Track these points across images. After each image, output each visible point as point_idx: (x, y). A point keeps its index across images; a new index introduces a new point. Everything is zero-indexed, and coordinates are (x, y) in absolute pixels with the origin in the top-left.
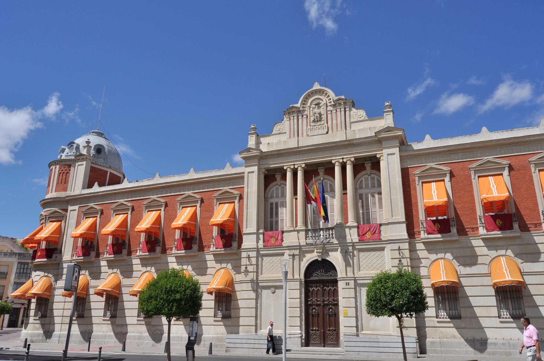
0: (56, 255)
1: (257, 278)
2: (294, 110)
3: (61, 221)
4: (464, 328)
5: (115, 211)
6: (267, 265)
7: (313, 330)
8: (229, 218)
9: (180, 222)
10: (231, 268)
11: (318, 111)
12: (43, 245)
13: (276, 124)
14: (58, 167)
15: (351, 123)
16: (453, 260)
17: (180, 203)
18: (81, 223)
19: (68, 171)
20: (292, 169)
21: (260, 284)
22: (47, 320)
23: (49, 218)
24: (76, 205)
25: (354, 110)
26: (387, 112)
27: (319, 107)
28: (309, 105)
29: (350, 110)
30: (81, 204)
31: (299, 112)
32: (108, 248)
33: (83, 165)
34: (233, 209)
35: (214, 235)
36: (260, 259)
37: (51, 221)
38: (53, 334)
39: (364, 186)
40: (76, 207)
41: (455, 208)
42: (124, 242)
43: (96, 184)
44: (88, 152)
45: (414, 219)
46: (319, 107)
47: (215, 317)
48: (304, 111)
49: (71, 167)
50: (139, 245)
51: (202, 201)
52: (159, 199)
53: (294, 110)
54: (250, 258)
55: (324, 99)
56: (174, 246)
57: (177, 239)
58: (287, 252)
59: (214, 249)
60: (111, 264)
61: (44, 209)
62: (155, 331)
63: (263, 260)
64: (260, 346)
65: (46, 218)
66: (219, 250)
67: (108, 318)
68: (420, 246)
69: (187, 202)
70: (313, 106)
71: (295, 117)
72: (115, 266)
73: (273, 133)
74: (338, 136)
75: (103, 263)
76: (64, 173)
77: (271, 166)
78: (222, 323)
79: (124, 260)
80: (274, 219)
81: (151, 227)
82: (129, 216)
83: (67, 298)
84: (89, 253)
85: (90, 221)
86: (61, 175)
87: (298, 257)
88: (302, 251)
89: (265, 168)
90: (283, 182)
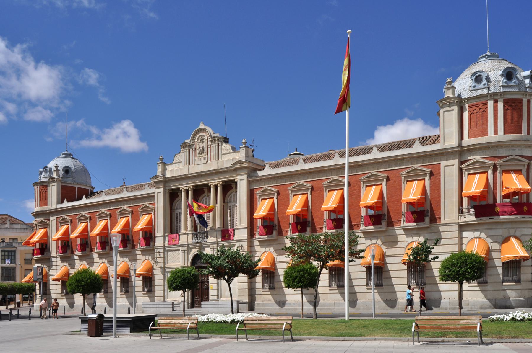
0: (47, 252)
1: (164, 266)
2: (186, 144)
4: (276, 295)
5: (79, 220)
6: (170, 257)
7: (196, 298)
11: (201, 145)
13: (176, 155)
14: (38, 187)
18: (77, 227)
19: (46, 190)
20: (214, 185)
21: (167, 270)
22: (385, 289)
23: (38, 226)
26: (242, 147)
27: (203, 142)
28: (196, 140)
29: (222, 145)
30: (384, 169)
31: (190, 146)
32: (78, 247)
33: (55, 185)
35: (325, 219)
36: (166, 253)
37: (40, 228)
39: (232, 201)
40: (55, 218)
42: (87, 242)
43: (65, 200)
46: (203, 142)
48: (193, 145)
49: (498, 102)
51: (388, 179)
52: (305, 184)
53: (186, 144)
55: (206, 136)
56: (257, 232)
58: (181, 248)
59: (140, 247)
60: (101, 256)
61: (35, 218)
63: (168, 253)
65: (36, 226)
66: (142, 247)
67: (124, 293)
68: (256, 243)
70: (199, 141)
72: (83, 259)
73: (174, 162)
74: (212, 166)
75: (76, 258)
76: (43, 192)
77: (172, 188)
80: (178, 225)
81: (483, 191)
82: (89, 224)
86: (42, 193)
87: (187, 252)
88: (189, 248)
89: (169, 189)
90: (209, 193)
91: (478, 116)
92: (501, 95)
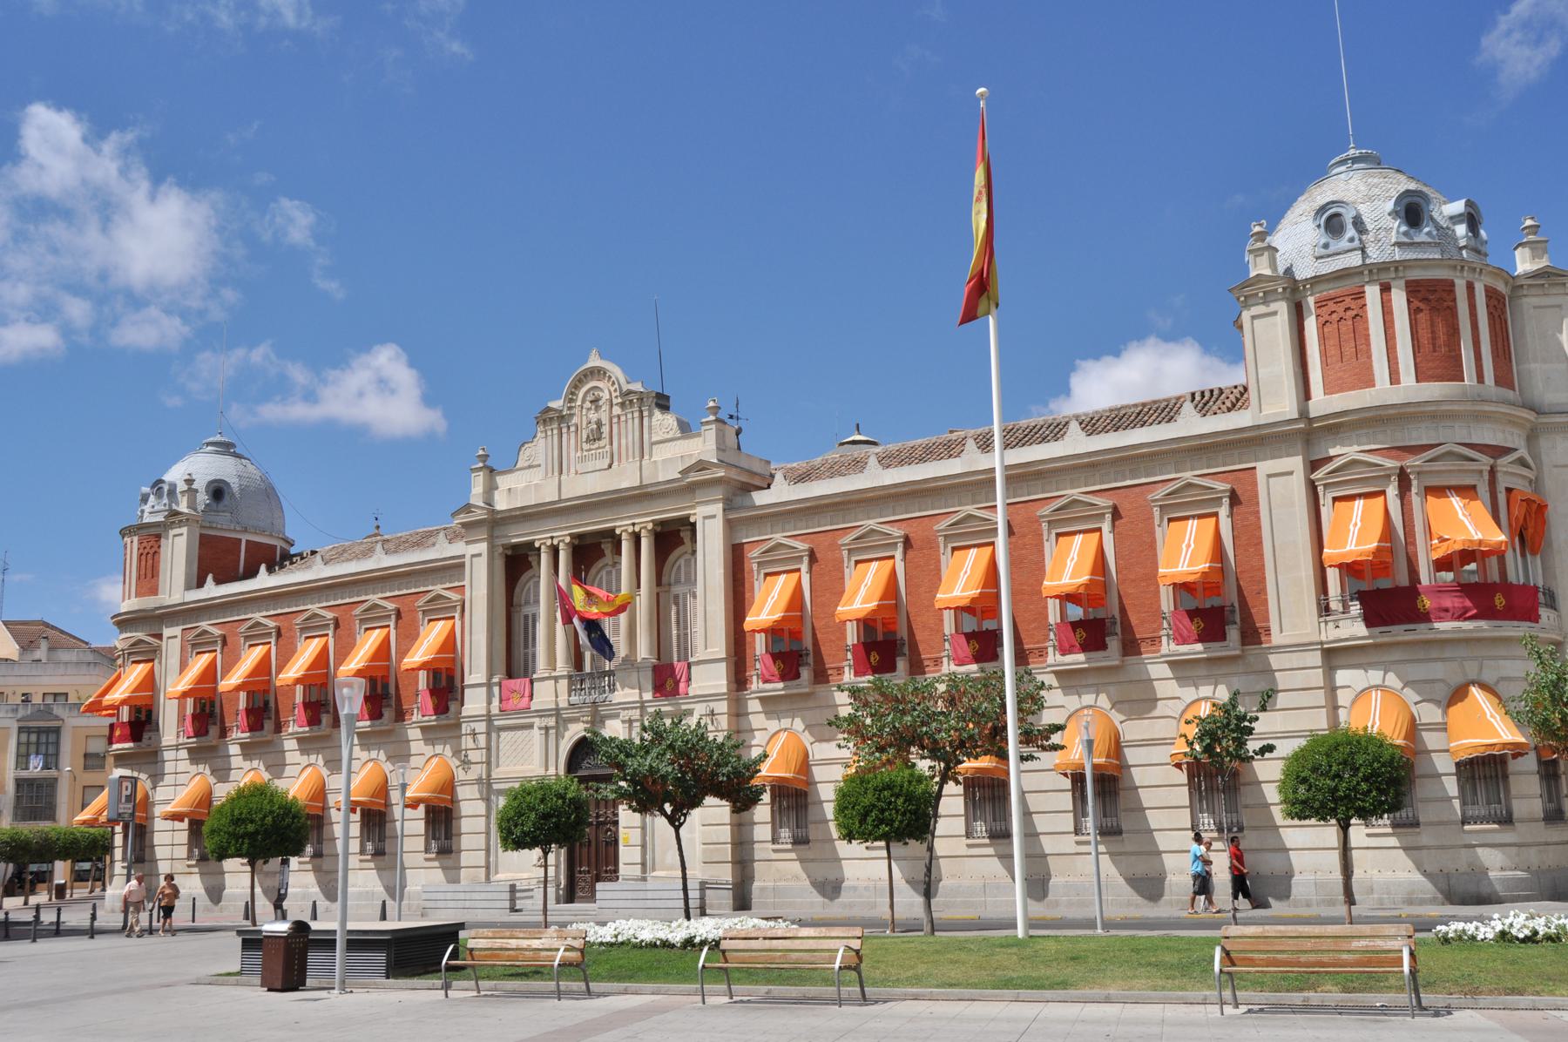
1: (489, 775)
3: (152, 660)
4: (812, 860)
5: (247, 638)
7: (580, 872)
8: (1383, 544)
9: (957, 593)
10: (450, 754)
11: (593, 416)
12: (125, 717)
13: (523, 445)
14: (136, 539)
15: (652, 444)
16: (1402, 689)
17: (361, 620)
21: (495, 787)
22: (1129, 843)
23: (129, 654)
24: (177, 625)
25: (657, 414)
26: (708, 423)
27: (598, 408)
28: (579, 403)
29: (651, 416)
34: (989, 564)
36: (494, 735)
37: (134, 662)
38: (1293, 882)
39: (683, 580)
40: (176, 631)
41: (813, 628)
42: (266, 703)
44: (192, 505)
45: (747, 651)
46: (598, 408)
47: (968, 838)
48: (572, 415)
50: (293, 711)
51: (1116, 514)
52: (886, 529)
53: (551, 415)
54: (713, 715)
56: (755, 672)
57: (853, 645)
59: (420, 716)
61: (121, 632)
62: (329, 882)
63: (499, 736)
64: (670, 904)
68: (754, 705)
69: (867, 548)
71: (555, 432)
72: (255, 754)
74: (626, 478)
75: (234, 749)
76: (148, 553)
78: (793, 855)
79: (269, 743)
80: (530, 651)
83: (176, 822)
84: (381, 712)
85: (204, 659)
86: (143, 557)
89: (503, 545)
91: (1343, 329)
92: (1397, 269)
